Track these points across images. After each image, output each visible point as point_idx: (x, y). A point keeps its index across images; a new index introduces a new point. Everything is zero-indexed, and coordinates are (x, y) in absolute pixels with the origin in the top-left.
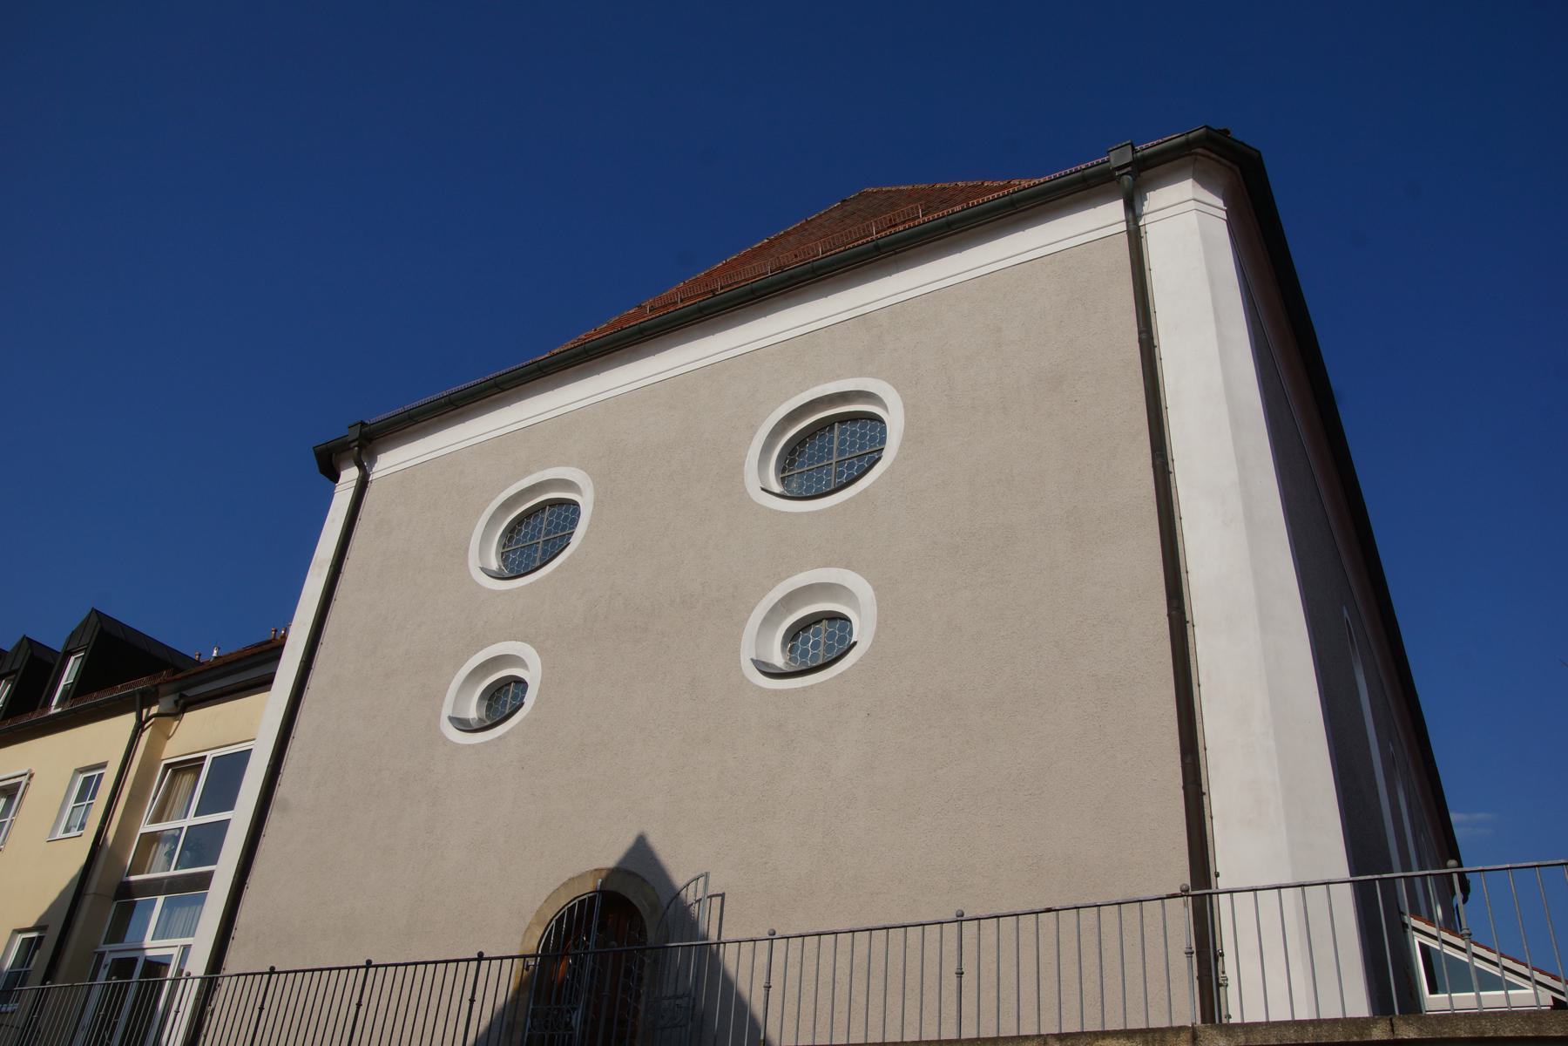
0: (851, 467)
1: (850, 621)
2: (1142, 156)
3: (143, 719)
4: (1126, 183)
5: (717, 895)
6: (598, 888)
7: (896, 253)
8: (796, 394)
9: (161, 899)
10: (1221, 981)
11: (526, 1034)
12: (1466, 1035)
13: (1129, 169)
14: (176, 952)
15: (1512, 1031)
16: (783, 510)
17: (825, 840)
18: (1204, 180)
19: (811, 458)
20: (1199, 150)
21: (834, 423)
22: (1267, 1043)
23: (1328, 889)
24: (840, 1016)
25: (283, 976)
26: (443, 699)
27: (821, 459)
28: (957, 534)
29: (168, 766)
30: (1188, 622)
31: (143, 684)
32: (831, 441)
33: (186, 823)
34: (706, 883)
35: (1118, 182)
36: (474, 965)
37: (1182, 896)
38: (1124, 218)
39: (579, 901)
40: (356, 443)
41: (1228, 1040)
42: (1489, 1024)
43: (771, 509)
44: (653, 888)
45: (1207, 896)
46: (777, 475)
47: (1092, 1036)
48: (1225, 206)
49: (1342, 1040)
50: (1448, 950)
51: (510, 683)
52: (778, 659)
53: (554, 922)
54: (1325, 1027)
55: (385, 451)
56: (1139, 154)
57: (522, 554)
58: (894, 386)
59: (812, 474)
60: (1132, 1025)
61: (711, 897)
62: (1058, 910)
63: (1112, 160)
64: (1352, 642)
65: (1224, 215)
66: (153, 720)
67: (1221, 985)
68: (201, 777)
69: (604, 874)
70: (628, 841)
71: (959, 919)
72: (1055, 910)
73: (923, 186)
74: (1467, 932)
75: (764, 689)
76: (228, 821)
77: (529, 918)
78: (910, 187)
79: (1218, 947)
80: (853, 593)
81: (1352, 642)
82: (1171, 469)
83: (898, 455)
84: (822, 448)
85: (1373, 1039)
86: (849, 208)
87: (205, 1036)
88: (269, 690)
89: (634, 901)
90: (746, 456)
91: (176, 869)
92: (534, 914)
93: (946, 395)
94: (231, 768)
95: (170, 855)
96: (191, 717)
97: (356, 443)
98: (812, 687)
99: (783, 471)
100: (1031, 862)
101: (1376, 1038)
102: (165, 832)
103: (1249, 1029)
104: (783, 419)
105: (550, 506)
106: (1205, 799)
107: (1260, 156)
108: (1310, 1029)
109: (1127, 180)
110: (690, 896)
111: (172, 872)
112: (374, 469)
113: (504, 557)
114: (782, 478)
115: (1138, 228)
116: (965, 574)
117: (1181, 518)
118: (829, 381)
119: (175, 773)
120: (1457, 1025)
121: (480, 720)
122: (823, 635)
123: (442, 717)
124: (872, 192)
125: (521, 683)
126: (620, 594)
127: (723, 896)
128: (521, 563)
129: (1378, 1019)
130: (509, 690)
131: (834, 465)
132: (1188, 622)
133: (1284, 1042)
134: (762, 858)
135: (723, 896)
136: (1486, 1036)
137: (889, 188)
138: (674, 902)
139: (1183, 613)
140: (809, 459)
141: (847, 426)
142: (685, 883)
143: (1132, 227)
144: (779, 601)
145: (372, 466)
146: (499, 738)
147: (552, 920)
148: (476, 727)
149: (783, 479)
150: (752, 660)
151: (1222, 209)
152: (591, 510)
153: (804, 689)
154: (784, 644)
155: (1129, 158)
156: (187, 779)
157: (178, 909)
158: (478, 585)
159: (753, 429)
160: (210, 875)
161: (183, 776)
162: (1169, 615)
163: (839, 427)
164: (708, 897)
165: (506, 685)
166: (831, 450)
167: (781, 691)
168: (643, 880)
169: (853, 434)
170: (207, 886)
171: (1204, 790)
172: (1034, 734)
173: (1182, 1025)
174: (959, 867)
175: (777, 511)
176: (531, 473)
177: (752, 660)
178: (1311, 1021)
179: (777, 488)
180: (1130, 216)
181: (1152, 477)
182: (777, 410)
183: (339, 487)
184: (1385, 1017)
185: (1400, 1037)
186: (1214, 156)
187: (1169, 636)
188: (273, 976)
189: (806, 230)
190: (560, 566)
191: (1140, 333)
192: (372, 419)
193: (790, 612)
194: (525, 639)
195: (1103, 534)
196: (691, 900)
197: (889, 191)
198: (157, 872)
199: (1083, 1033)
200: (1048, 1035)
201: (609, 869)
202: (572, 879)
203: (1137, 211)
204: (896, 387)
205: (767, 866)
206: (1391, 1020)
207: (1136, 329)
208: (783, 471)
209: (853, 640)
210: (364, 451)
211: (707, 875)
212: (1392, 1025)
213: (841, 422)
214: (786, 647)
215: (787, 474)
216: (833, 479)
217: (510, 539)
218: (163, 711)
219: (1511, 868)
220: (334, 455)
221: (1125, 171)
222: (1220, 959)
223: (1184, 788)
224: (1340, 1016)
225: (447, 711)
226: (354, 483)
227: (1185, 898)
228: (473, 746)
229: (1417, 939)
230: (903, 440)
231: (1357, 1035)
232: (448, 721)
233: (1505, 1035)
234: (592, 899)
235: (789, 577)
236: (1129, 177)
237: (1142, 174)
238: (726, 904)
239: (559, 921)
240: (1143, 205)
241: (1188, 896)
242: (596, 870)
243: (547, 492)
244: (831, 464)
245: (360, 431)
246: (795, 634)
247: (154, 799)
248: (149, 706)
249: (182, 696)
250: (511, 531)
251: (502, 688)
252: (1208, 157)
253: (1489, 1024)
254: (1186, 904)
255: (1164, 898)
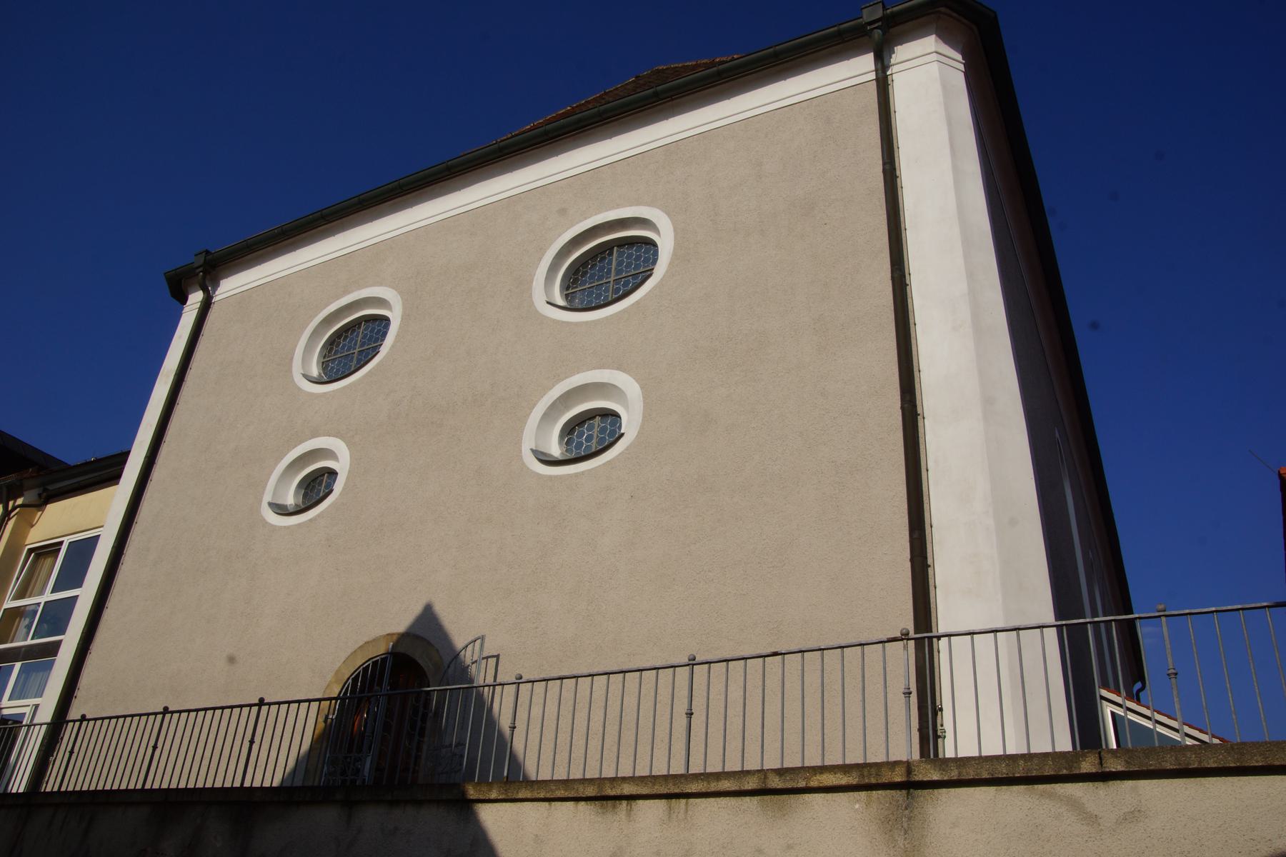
0: (626, 284)
1: (620, 417)
2: (892, 13)
3: (10, 508)
4: (876, 36)
5: (493, 656)
6: (390, 650)
7: (673, 100)
8: (581, 221)
9: (18, 665)
10: (939, 733)
11: (323, 780)
12: (1172, 767)
13: (880, 23)
14: (27, 710)
15: (1214, 762)
16: (564, 320)
17: (589, 608)
18: (946, 37)
19: (592, 277)
20: (943, 9)
21: (613, 247)
22: (979, 777)
23: (1042, 632)
24: (578, 753)
25: (92, 723)
26: (264, 488)
27: (600, 278)
28: (716, 339)
29: (31, 551)
30: (919, 415)
31: (11, 478)
32: (610, 263)
33: (42, 599)
34: (482, 645)
35: (870, 37)
36: (255, 709)
37: (902, 640)
38: (873, 68)
39: (373, 662)
40: (201, 269)
41: (942, 774)
42: (1194, 756)
43: (554, 320)
44: (437, 650)
45: (926, 640)
46: (561, 292)
47: (810, 771)
48: (963, 59)
49: (1052, 773)
50: (1131, 716)
51: (324, 475)
52: (556, 451)
53: (350, 681)
54: (1036, 761)
55: (227, 277)
56: (888, 11)
57: (340, 363)
58: (666, 213)
59: (593, 291)
60: (850, 760)
61: (487, 658)
62: (784, 654)
63: (865, 16)
64: (1062, 462)
65: (962, 67)
66: (18, 510)
67: (940, 737)
68: (58, 561)
69: (395, 638)
70: (417, 609)
71: (691, 662)
72: (781, 654)
73: (705, 61)
74: (1173, 671)
75: (541, 475)
76: (77, 597)
77: (330, 677)
78: (694, 63)
79: (938, 703)
80: (623, 392)
81: (1062, 462)
82: (908, 282)
83: (667, 272)
84: (602, 269)
85: (1082, 772)
86: (641, 82)
87: (47, 783)
88: (117, 483)
89: (420, 662)
90: (534, 275)
91: (32, 639)
92: (334, 672)
93: (711, 220)
94: (84, 550)
95: (29, 627)
96: (51, 508)
97: (201, 269)
98: (583, 473)
99: (568, 288)
100: (772, 627)
101: (1085, 771)
102: (28, 607)
103: (962, 764)
104: (568, 242)
105: (365, 321)
106: (930, 570)
107: (996, 17)
108: (1021, 762)
109: (878, 34)
110: (468, 657)
111: (29, 642)
112: (217, 293)
113: (324, 365)
114: (566, 294)
115: (886, 77)
116: (722, 374)
117: (915, 324)
118: (610, 210)
119: (38, 557)
120: (1163, 758)
121: (296, 505)
122: (596, 430)
123: (263, 503)
124: (663, 69)
125: (332, 474)
126: (420, 395)
127: (497, 657)
128: (338, 370)
129: (1088, 753)
130: (323, 480)
131: (612, 282)
132: (919, 415)
133: (996, 776)
134: (534, 623)
135: (497, 657)
136: (1190, 767)
137: (677, 65)
138: (454, 662)
139: (915, 406)
140: (590, 278)
141: (625, 250)
142: (464, 645)
143: (880, 75)
144: (557, 399)
145: (214, 291)
146: (311, 520)
147: (349, 679)
148: (291, 511)
149: (567, 296)
150: (532, 450)
151: (961, 63)
152: (399, 323)
153: (576, 475)
154: (561, 436)
155: (879, 13)
156: (49, 561)
157: (34, 674)
158: (299, 389)
159: (542, 251)
160: (59, 643)
161: (45, 559)
162: (902, 408)
163: (617, 251)
164: (483, 658)
165: (321, 476)
166: (609, 270)
167: (556, 477)
168: (429, 643)
169: (630, 256)
170: (55, 654)
171: (929, 563)
172: (778, 513)
173: (899, 759)
174: (707, 631)
175: (559, 321)
176: (349, 293)
177: (532, 450)
178: (1023, 756)
179: (561, 302)
180: (879, 65)
181: (891, 289)
182: (563, 236)
183: (186, 309)
184: (1094, 751)
185: (1108, 770)
186: (955, 15)
187: (902, 427)
188: (84, 722)
189: (604, 99)
190: (370, 371)
191: (884, 164)
192: (216, 248)
193: (568, 408)
194: (337, 435)
195: (846, 339)
196: (468, 661)
197: (676, 67)
198: (19, 641)
199: (803, 768)
200: (768, 770)
201: (398, 634)
202: (367, 643)
203: (886, 63)
204: (668, 214)
205: (537, 630)
206: (1100, 753)
207: (881, 162)
208: (568, 288)
209: (622, 431)
210: (208, 277)
211: (482, 638)
212: (1100, 758)
213: (620, 246)
214: (564, 440)
215: (570, 291)
216: (610, 295)
217: (330, 351)
218: (27, 502)
219: (1216, 611)
220: (183, 281)
221: (876, 25)
222: (939, 713)
223: (912, 560)
224: (1050, 750)
225: (267, 497)
226: (198, 305)
227: (905, 641)
228: (288, 528)
229: (1108, 709)
230: (672, 259)
231: (1066, 769)
232: (267, 505)
233: (1209, 766)
234: (384, 660)
235: (566, 378)
236: (879, 31)
237: (891, 30)
238: (500, 664)
239: (355, 680)
240: (891, 57)
241: (908, 639)
242: (388, 635)
243: (362, 310)
244: (610, 282)
245: (205, 260)
246: (570, 429)
247: (18, 579)
248: (15, 499)
249: (45, 490)
250: (332, 343)
251: (316, 478)
252: (951, 16)
253: (1194, 756)
254: (906, 647)
255: (885, 642)
